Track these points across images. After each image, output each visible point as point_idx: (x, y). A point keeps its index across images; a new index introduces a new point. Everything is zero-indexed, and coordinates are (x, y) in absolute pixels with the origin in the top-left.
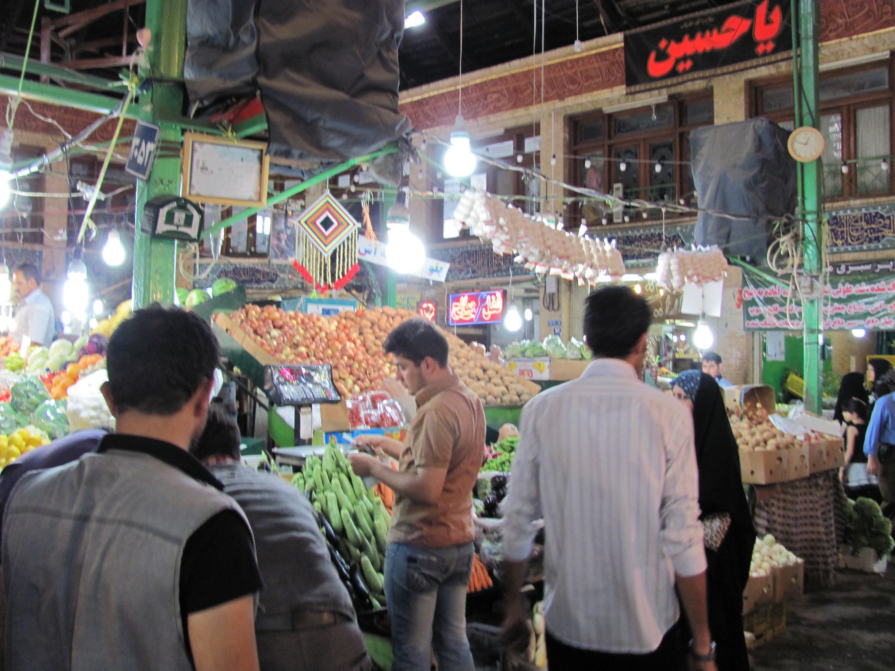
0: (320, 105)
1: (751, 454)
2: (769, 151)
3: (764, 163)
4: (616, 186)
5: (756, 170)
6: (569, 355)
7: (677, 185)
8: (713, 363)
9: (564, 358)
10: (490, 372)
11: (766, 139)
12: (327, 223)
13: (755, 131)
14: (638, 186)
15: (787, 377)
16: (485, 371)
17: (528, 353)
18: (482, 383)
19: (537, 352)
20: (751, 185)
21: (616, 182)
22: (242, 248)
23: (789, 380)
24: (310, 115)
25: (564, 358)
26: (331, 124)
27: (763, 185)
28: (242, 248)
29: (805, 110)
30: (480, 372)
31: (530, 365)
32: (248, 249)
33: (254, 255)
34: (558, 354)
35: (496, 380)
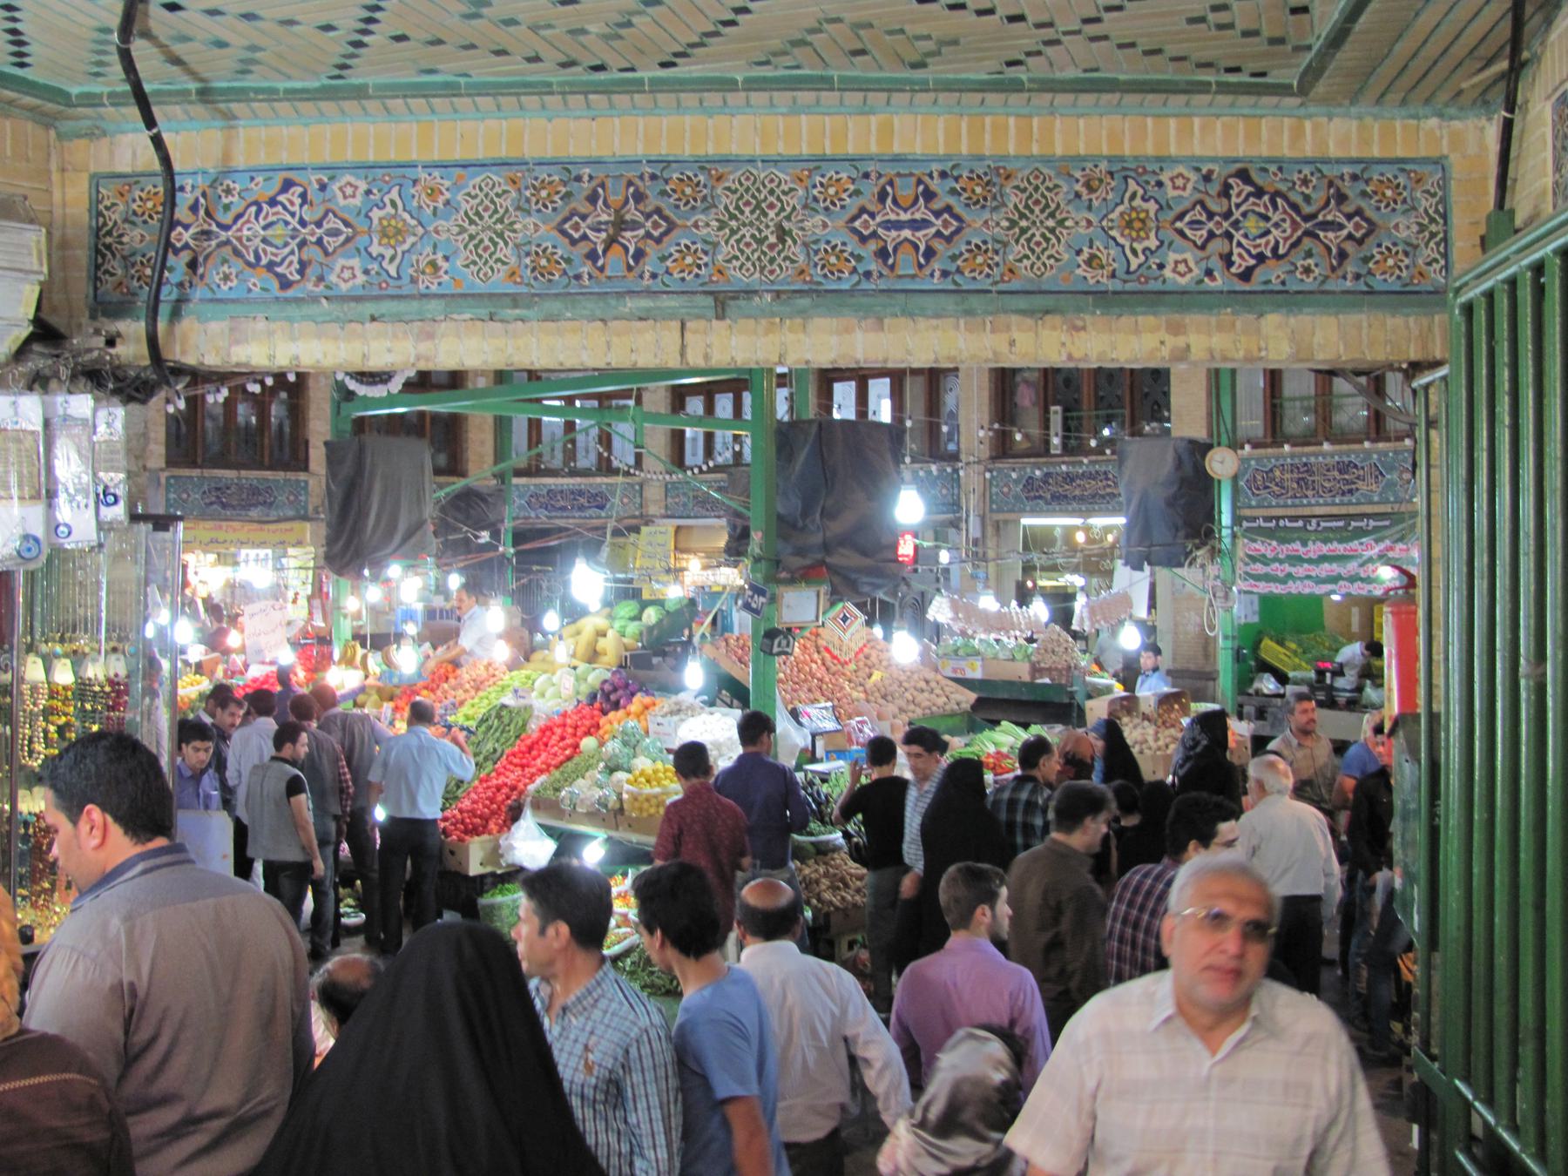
0: (859, 570)
1: (1154, 757)
2: (1188, 469)
3: (1183, 482)
4: (1053, 408)
5: (1175, 488)
6: (1001, 656)
7: (1127, 412)
8: (1151, 654)
9: (995, 658)
10: (933, 684)
11: (1185, 457)
12: (845, 619)
13: (1176, 451)
14: (1080, 410)
15: (1260, 641)
16: (927, 682)
17: (961, 652)
18: (926, 695)
19: (969, 651)
20: (1171, 503)
21: (1055, 404)
22: (557, 462)
23: (1262, 645)
24: (853, 576)
25: (995, 658)
26: (865, 579)
27: (1182, 502)
28: (557, 462)
29: (1222, 429)
30: (922, 685)
31: (963, 664)
32: (566, 463)
33: (574, 473)
34: (989, 653)
35: (938, 691)
